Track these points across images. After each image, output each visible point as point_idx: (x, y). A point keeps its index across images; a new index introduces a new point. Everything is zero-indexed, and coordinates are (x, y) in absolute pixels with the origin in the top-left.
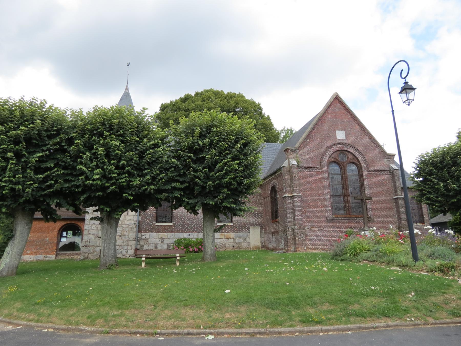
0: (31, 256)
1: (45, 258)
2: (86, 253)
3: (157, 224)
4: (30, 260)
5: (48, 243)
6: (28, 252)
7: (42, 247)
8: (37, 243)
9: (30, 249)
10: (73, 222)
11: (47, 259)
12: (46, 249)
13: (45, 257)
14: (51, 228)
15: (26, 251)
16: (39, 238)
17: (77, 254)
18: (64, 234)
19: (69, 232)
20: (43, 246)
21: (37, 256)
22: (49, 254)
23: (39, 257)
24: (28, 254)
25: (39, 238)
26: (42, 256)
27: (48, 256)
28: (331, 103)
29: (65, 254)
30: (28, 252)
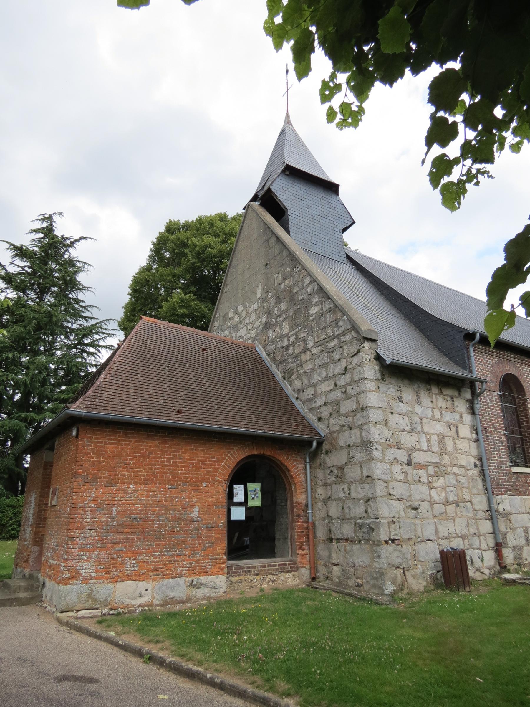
0: (142, 585)
1: (194, 591)
2: (398, 568)
3: (515, 469)
4: (141, 601)
5: (198, 529)
6: (129, 568)
7: (179, 545)
8: (160, 527)
9: (135, 555)
10: (268, 452)
11: (201, 593)
12: (194, 551)
13: (192, 585)
14: (203, 470)
15: (123, 563)
16: (167, 509)
17: (283, 569)
18: (239, 489)
19: (251, 486)
20: (181, 543)
21: (166, 582)
22: (206, 573)
23: (172, 588)
24: (129, 577)
25: (167, 509)
26: (181, 581)
27: (204, 579)
28: (326, 293)
29: (248, 571)
30: (129, 568)
